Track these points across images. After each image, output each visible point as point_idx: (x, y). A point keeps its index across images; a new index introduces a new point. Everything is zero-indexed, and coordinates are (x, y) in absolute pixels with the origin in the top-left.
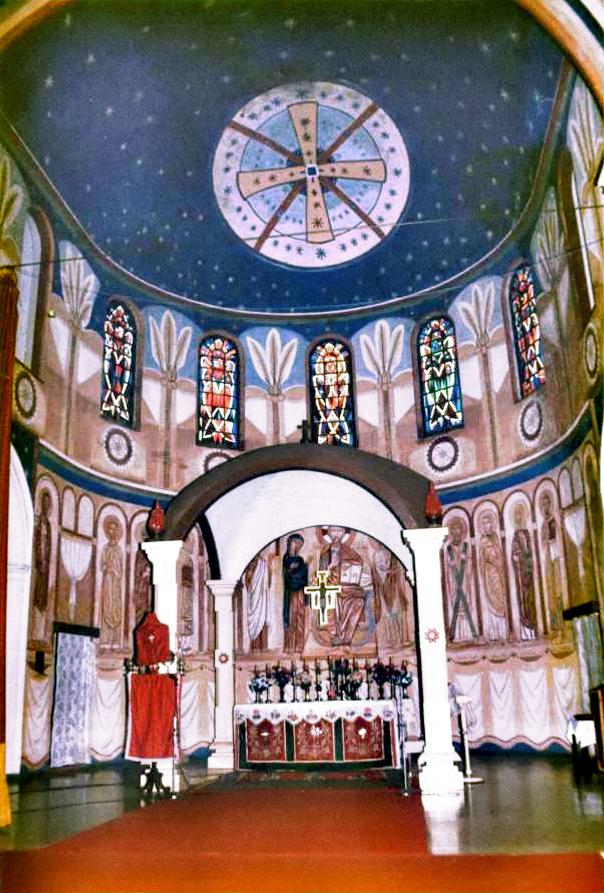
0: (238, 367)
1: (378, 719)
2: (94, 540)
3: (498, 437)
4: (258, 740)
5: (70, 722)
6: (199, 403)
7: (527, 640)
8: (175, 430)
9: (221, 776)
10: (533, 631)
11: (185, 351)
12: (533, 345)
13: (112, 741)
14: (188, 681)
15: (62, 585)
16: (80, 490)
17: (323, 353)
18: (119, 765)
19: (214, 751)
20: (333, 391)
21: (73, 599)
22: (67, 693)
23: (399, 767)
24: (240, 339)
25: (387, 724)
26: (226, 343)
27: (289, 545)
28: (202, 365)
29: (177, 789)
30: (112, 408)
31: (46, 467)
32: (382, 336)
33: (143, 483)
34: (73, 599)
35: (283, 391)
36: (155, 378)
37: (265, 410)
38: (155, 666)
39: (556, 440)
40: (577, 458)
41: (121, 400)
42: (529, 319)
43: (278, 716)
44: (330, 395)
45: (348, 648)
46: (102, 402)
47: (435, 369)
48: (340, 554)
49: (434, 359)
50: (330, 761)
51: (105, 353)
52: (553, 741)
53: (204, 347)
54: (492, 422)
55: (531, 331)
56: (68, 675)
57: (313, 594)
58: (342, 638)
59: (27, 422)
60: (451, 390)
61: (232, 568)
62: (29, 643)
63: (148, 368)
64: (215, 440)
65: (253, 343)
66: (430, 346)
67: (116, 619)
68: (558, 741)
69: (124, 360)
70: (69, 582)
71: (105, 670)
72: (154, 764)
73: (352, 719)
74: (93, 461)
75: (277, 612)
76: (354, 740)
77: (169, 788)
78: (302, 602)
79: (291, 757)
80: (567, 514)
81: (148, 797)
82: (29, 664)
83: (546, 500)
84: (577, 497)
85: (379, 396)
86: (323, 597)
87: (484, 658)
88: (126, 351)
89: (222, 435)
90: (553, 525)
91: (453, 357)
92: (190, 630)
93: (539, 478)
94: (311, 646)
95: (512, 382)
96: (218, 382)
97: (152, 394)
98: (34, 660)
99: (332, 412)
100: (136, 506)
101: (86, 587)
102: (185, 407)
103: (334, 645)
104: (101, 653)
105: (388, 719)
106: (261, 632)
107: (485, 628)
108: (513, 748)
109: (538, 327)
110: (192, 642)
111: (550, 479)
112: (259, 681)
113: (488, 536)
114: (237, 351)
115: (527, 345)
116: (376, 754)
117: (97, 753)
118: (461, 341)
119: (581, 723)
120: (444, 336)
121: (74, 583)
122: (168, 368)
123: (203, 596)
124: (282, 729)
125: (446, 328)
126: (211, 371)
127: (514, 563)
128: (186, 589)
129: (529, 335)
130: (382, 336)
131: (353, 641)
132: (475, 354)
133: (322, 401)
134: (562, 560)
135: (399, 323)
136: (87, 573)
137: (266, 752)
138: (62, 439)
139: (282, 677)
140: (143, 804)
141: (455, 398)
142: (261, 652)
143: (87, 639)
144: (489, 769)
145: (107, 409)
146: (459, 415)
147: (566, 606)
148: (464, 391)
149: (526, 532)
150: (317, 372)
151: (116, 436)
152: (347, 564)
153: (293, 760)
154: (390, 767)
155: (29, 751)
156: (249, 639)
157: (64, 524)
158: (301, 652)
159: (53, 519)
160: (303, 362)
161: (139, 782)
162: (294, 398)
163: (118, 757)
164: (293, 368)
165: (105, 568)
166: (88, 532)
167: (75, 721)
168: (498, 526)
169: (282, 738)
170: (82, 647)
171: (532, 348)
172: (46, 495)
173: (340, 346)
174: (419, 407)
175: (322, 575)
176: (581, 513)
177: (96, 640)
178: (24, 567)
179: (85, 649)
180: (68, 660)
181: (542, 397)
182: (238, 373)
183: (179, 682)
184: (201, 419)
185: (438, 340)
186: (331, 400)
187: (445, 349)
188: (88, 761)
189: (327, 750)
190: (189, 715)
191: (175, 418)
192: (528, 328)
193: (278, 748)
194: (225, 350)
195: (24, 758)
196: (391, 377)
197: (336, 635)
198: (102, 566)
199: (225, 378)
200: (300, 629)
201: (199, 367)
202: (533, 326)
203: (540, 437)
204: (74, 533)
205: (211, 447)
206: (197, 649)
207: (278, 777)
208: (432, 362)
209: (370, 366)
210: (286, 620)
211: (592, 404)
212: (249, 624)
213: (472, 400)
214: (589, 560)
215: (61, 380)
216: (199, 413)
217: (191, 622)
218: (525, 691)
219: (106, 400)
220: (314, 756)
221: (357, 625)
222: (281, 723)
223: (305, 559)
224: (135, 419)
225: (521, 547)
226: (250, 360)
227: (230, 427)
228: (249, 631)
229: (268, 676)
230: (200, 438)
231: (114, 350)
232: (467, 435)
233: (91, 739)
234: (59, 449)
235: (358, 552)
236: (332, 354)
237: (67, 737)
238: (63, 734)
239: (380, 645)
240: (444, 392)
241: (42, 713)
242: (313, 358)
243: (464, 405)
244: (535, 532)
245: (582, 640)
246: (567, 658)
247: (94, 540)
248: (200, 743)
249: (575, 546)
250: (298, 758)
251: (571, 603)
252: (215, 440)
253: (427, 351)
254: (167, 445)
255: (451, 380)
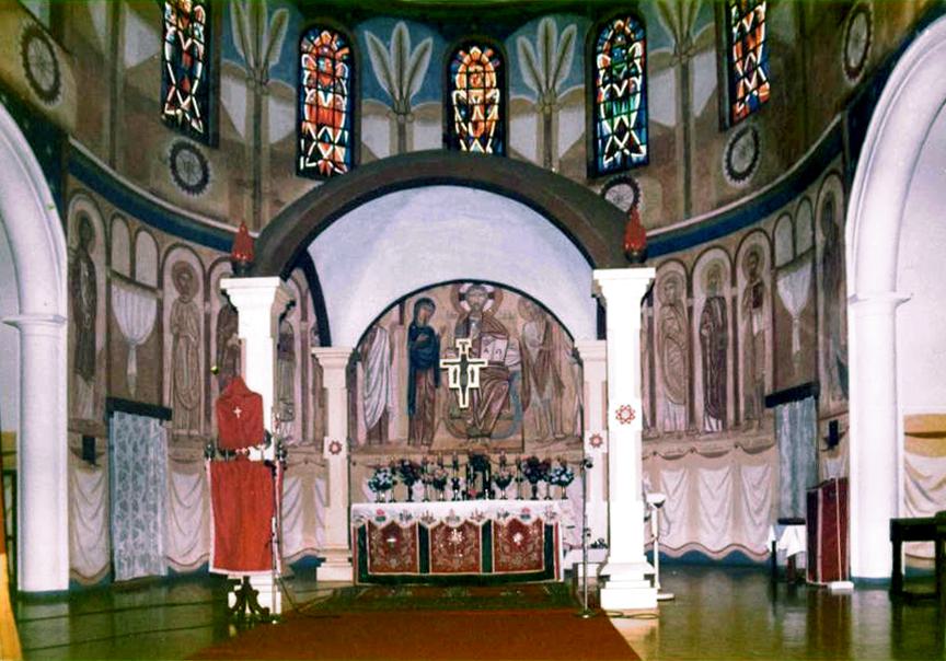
0: (352, 72)
1: (538, 522)
2: (160, 292)
3: (694, 176)
4: (383, 547)
5: (138, 524)
6: (300, 119)
7: (712, 432)
8: (268, 151)
9: (335, 591)
10: (720, 423)
11: (280, 43)
12: (755, 51)
13: (195, 545)
14: (291, 476)
15: (116, 350)
16: (138, 223)
17: (466, 59)
18: (201, 576)
19: (323, 560)
20: (478, 112)
21: (132, 369)
22: (131, 490)
23: (562, 580)
24: (355, 33)
25: (549, 529)
26: (336, 37)
27: (416, 313)
28: (304, 65)
29: (279, 611)
30: (179, 111)
31: (80, 178)
32: (547, 38)
33: (225, 221)
34: (132, 369)
35: (413, 109)
36: (237, 76)
37: (387, 136)
38: (244, 450)
39: (777, 176)
40: (809, 200)
41: (191, 102)
42: (752, 14)
43: (409, 517)
44: (474, 118)
45: (487, 440)
46: (164, 101)
47: (615, 86)
48: (480, 325)
49: (614, 72)
50: (476, 573)
51: (165, 31)
52: (735, 548)
53: (305, 40)
54: (687, 157)
55: (753, 29)
56: (131, 465)
57: (451, 369)
58: (480, 428)
59: (48, 108)
60: (634, 116)
61: (347, 329)
62: (70, 420)
63: (227, 61)
64: (322, 171)
65: (372, 39)
66: (611, 55)
67: (193, 398)
68: (741, 549)
69: (193, 46)
70: (125, 345)
71: (180, 463)
72: (247, 579)
73: (504, 522)
74: (155, 184)
75: (400, 393)
76: (507, 548)
77: (267, 609)
78: (432, 383)
79: (425, 568)
80: (780, 275)
81: (241, 621)
82: (73, 450)
83: (753, 259)
84: (801, 249)
85: (539, 120)
86: (464, 372)
87: (655, 453)
88: (196, 33)
89: (331, 165)
90: (760, 289)
91: (640, 71)
92: (291, 414)
93: (745, 230)
94: (442, 437)
95: (720, 103)
96: (326, 92)
97: (235, 99)
98: (80, 445)
99: (476, 141)
100: (216, 252)
101: (151, 355)
102: (279, 121)
103: (469, 437)
104: (174, 440)
105: (552, 522)
106: (380, 420)
107: (659, 419)
108: (683, 557)
109: (763, 26)
110: (293, 430)
111: (760, 230)
112: (380, 476)
113: (671, 305)
114: (350, 50)
115: (745, 52)
116: (534, 565)
117: (318, 551)
118: (653, 49)
119: (790, 529)
120: (630, 42)
121: (133, 347)
122: (257, 64)
123: (307, 371)
124: (414, 535)
125: (633, 31)
126: (315, 74)
127: (702, 338)
128: (285, 364)
129: (749, 38)
130: (547, 38)
131: (494, 432)
132: (671, 65)
133: (463, 125)
134: (768, 335)
135: (572, 22)
136: (153, 333)
137: (394, 562)
138: (106, 142)
139: (410, 473)
140: (232, 630)
141: (638, 127)
142: (381, 443)
143: (154, 422)
144: (734, 587)
145: (172, 112)
146: (643, 149)
147: (768, 390)
148: (651, 117)
149: (722, 299)
150: (458, 86)
151: (186, 152)
152: (490, 338)
153: (428, 571)
154: (550, 581)
155: (80, 564)
156: (365, 428)
157: (116, 266)
158: (429, 445)
159: (98, 257)
160: (440, 70)
161: (227, 601)
162: (427, 120)
163: (201, 567)
164: (426, 78)
165: (175, 330)
166: (152, 281)
167: (144, 522)
168: (685, 291)
169: (414, 545)
170: (148, 432)
171: (752, 55)
172: (84, 221)
173: (489, 52)
174: (591, 137)
175: (463, 345)
176: (804, 274)
177: (169, 424)
178: (57, 320)
179: (153, 434)
180: (130, 448)
181: (761, 120)
182: (352, 81)
183: (277, 471)
184: (303, 142)
185: (622, 47)
186: (475, 125)
187: (631, 59)
188: (164, 572)
189: (409, 560)
190: (292, 517)
191: (267, 135)
192: (748, 28)
193: (409, 557)
194: (335, 47)
195: (73, 570)
196: (556, 96)
197: (474, 425)
198: (171, 328)
199: (334, 87)
200: (429, 417)
201: (300, 70)
202: (756, 24)
203: (752, 175)
204: (131, 281)
205: (317, 179)
206: (300, 439)
207: (409, 593)
208: (611, 77)
209: (528, 81)
210: (411, 405)
211: (846, 122)
212: (365, 409)
213: (661, 126)
214: (811, 331)
215: (99, 57)
216: (300, 133)
217: (292, 404)
218: (703, 493)
219: (169, 98)
220: (456, 566)
221: (500, 414)
222: (413, 528)
223: (437, 331)
224: (211, 132)
225: (714, 320)
226: (370, 63)
227: (341, 153)
228: (365, 417)
229: (393, 473)
230: (302, 167)
231: (178, 29)
232: (650, 175)
233: (166, 547)
234: (100, 157)
235: (503, 322)
236: (479, 62)
237: (135, 544)
238: (130, 541)
239: (526, 438)
240: (625, 118)
241: (96, 514)
242: (454, 66)
243: (650, 136)
244: (734, 300)
245: (788, 430)
246: (765, 454)
247: (160, 292)
248: (306, 549)
249: (791, 317)
250: (433, 571)
251: (775, 383)
252: (322, 171)
253: (605, 61)
254: (257, 171)
255: (636, 101)
